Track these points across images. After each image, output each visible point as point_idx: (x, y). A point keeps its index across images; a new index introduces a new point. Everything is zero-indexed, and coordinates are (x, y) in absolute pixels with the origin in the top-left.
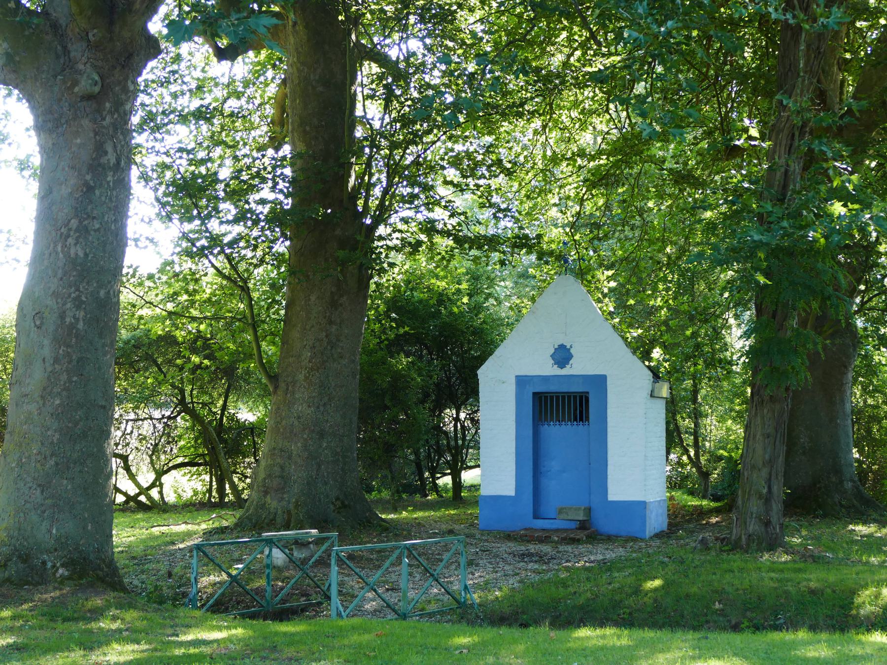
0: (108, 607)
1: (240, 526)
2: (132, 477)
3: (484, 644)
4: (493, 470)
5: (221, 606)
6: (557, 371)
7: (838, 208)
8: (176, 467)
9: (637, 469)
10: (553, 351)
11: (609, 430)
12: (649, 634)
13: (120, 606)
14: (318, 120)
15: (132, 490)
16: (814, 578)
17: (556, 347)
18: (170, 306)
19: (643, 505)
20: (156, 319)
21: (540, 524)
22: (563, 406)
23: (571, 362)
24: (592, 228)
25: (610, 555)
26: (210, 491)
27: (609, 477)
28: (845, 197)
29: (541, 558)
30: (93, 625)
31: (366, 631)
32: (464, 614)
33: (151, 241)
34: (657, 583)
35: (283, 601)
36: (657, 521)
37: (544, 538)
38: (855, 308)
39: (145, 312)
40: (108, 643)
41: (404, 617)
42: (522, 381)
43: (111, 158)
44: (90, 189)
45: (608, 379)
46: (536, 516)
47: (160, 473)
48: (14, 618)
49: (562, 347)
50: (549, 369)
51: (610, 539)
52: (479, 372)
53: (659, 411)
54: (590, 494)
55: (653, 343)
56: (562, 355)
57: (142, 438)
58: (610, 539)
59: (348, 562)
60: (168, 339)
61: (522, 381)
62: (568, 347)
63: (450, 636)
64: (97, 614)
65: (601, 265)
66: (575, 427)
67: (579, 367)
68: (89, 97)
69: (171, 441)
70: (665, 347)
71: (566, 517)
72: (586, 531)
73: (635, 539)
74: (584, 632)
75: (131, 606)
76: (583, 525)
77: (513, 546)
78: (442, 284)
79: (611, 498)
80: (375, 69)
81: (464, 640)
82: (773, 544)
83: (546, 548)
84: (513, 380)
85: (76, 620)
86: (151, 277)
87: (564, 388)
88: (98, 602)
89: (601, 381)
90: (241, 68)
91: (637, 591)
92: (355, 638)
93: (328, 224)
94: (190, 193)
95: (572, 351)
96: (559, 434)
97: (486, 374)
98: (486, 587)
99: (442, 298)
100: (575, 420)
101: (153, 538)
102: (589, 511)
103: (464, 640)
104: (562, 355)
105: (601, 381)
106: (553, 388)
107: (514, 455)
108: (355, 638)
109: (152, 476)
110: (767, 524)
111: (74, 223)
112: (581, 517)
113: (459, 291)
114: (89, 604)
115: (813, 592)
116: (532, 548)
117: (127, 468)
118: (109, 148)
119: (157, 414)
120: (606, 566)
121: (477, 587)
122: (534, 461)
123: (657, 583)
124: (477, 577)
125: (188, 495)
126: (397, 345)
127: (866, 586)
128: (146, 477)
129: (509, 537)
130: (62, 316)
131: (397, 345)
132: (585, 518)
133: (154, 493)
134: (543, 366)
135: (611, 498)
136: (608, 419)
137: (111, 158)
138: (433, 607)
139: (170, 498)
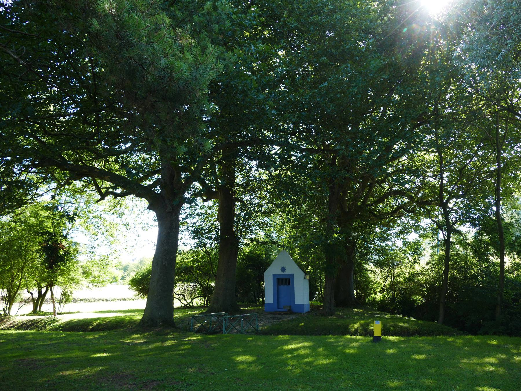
0: (171, 332)
1: (207, 312)
2: (185, 300)
3: (254, 340)
4: (269, 298)
5: (199, 331)
6: (282, 273)
7: (335, 235)
8: (197, 297)
9: (301, 296)
12: (295, 336)
13: (174, 332)
14: (226, 215)
15: (186, 303)
16: (340, 322)
18: (192, 259)
19: (303, 305)
20: (188, 262)
21: (279, 310)
22: (284, 282)
24: (295, 239)
25: (294, 317)
26: (204, 304)
28: (337, 233)
29: (278, 318)
30: (166, 337)
31: (229, 337)
32: (257, 332)
33: (186, 243)
34: (303, 324)
35: (214, 330)
36: (307, 309)
37: (280, 313)
39: (186, 261)
40: (167, 341)
41: (242, 333)
43: (174, 226)
44: (169, 233)
47: (192, 299)
48: (148, 335)
49: (283, 267)
51: (295, 313)
52: (264, 274)
53: (307, 283)
54: (125, 299)
55: (309, 265)
56: (283, 269)
57: (188, 290)
58: (295, 313)
60: (192, 267)
63: (247, 338)
64: (168, 334)
65: (296, 247)
67: (287, 272)
68: (169, 212)
69: (195, 291)
70: (312, 267)
72: (290, 311)
73: (301, 313)
74: (281, 336)
75: (176, 332)
76: (289, 310)
77: (272, 316)
78: (259, 252)
80: (239, 204)
81: (250, 339)
82: (332, 314)
83: (280, 316)
85: (162, 335)
86: (187, 252)
87: (284, 277)
88: (169, 331)
89: (292, 275)
90: (210, 203)
91: (298, 326)
92: (225, 338)
93: (228, 239)
94: (197, 233)
96: (283, 288)
97: (265, 274)
98: (263, 326)
99: (259, 256)
101: (187, 315)
102: (290, 306)
103: (250, 339)
104: (283, 269)
105: (292, 275)
106: (281, 277)
108: (225, 338)
109: (191, 300)
110: (331, 309)
111: (166, 241)
113: (262, 254)
114: (166, 332)
115: (339, 326)
116: (276, 316)
117: (184, 298)
118: (174, 224)
119: (192, 284)
120: (292, 320)
121: (261, 326)
122: (277, 295)
123: (303, 324)
124: (262, 323)
125: (199, 304)
126: (248, 267)
127: (351, 324)
128: (189, 301)
129: (271, 313)
130: (162, 263)
131: (248, 267)
133: (191, 304)
134: (279, 272)
137: (174, 226)
138: (250, 331)
139: (195, 304)
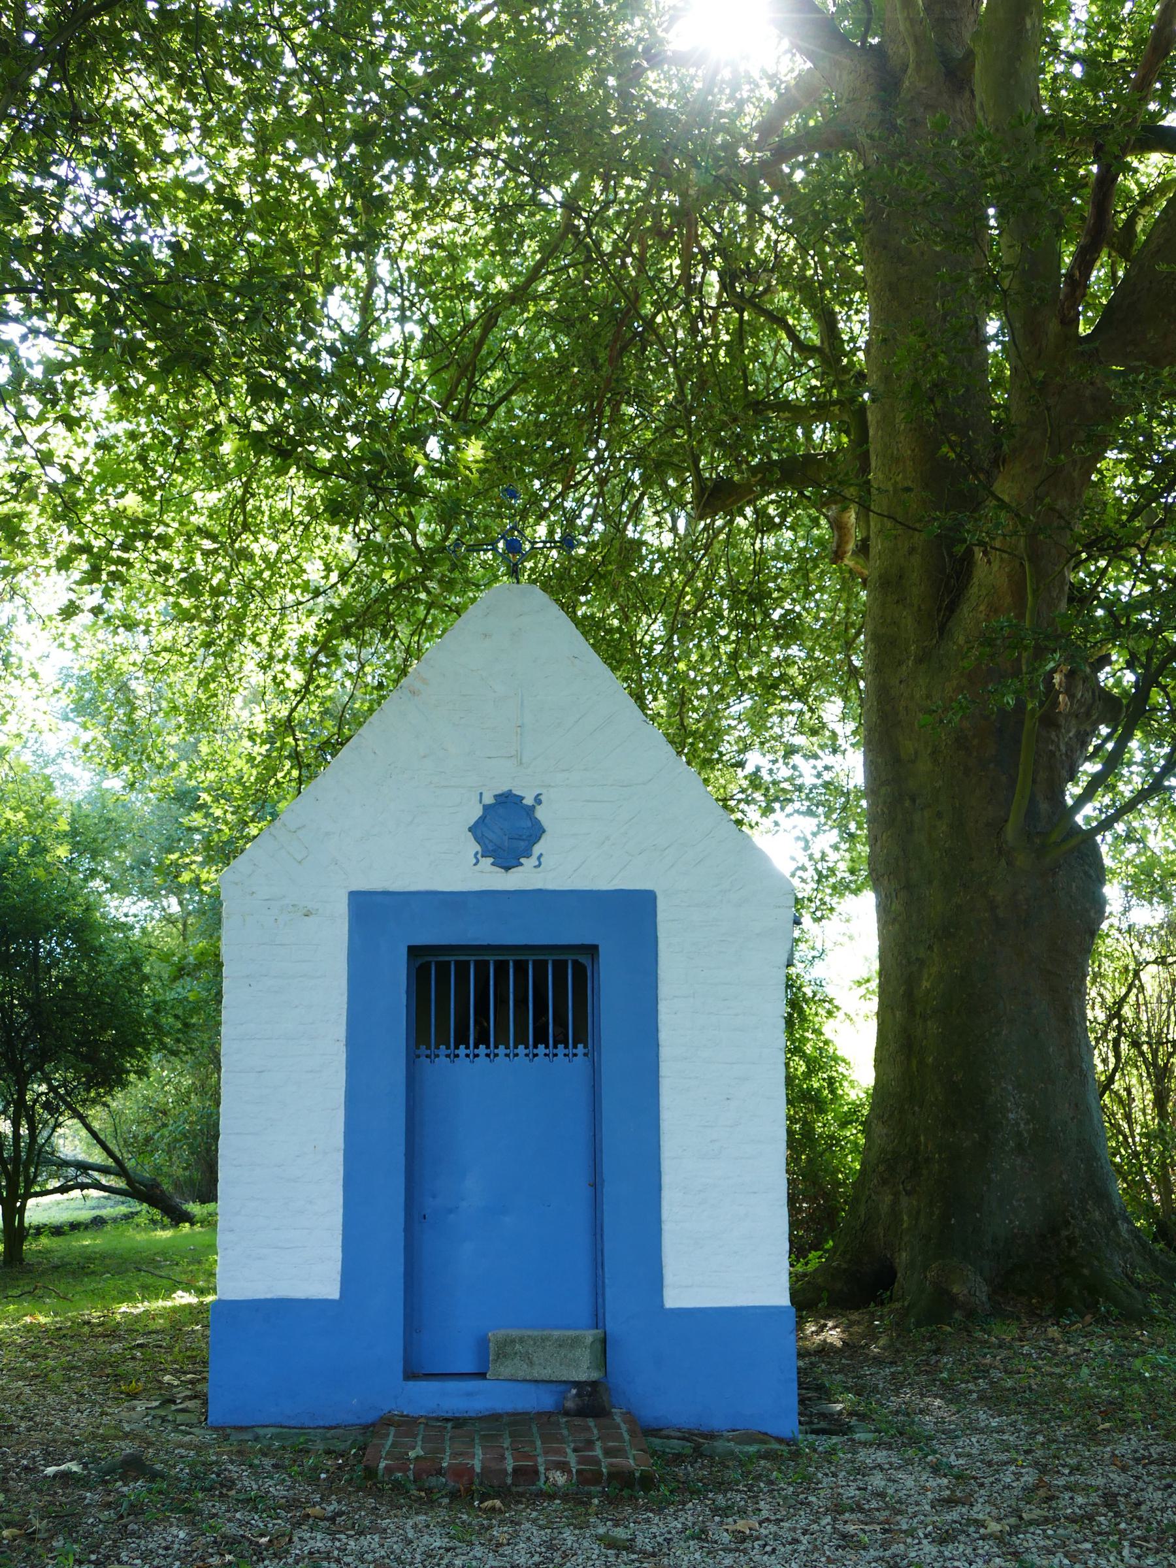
10: (477, 812)
11: (665, 1069)
17: (489, 800)
21: (429, 1398)
23: (537, 849)
27: (667, 1227)
38: (345, 237)
42: (368, 909)
45: (354, 889)
46: (411, 1374)
49: (507, 803)
50: (464, 871)
56: (508, 828)
59: (577, 1333)
61: (368, 909)
62: (529, 801)
66: (482, 1061)
71: (523, 1370)
79: (673, 1299)
84: (342, 907)
89: (636, 910)
95: (541, 814)
96: (496, 1087)
100: (521, 1039)
104: (508, 828)
105: (636, 910)
107: (339, 1158)
112: (584, 1372)
122: (404, 1180)
132: (595, 1375)
135: (673, 1299)
136: (663, 1036)
